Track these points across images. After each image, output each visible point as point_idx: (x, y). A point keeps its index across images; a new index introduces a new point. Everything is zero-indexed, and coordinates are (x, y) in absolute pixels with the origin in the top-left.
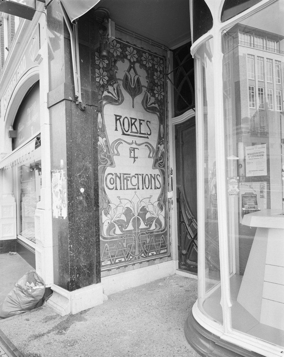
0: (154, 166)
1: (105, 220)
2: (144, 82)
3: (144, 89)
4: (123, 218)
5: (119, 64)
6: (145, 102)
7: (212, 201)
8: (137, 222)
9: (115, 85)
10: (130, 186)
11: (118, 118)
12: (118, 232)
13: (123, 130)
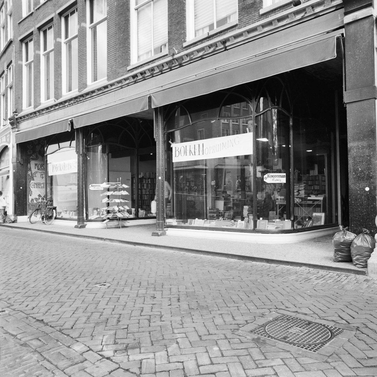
1: (30, 198)
4: (38, 197)
5: (37, 147)
9: (35, 154)
10: (40, 187)
11: (36, 165)
12: (35, 202)
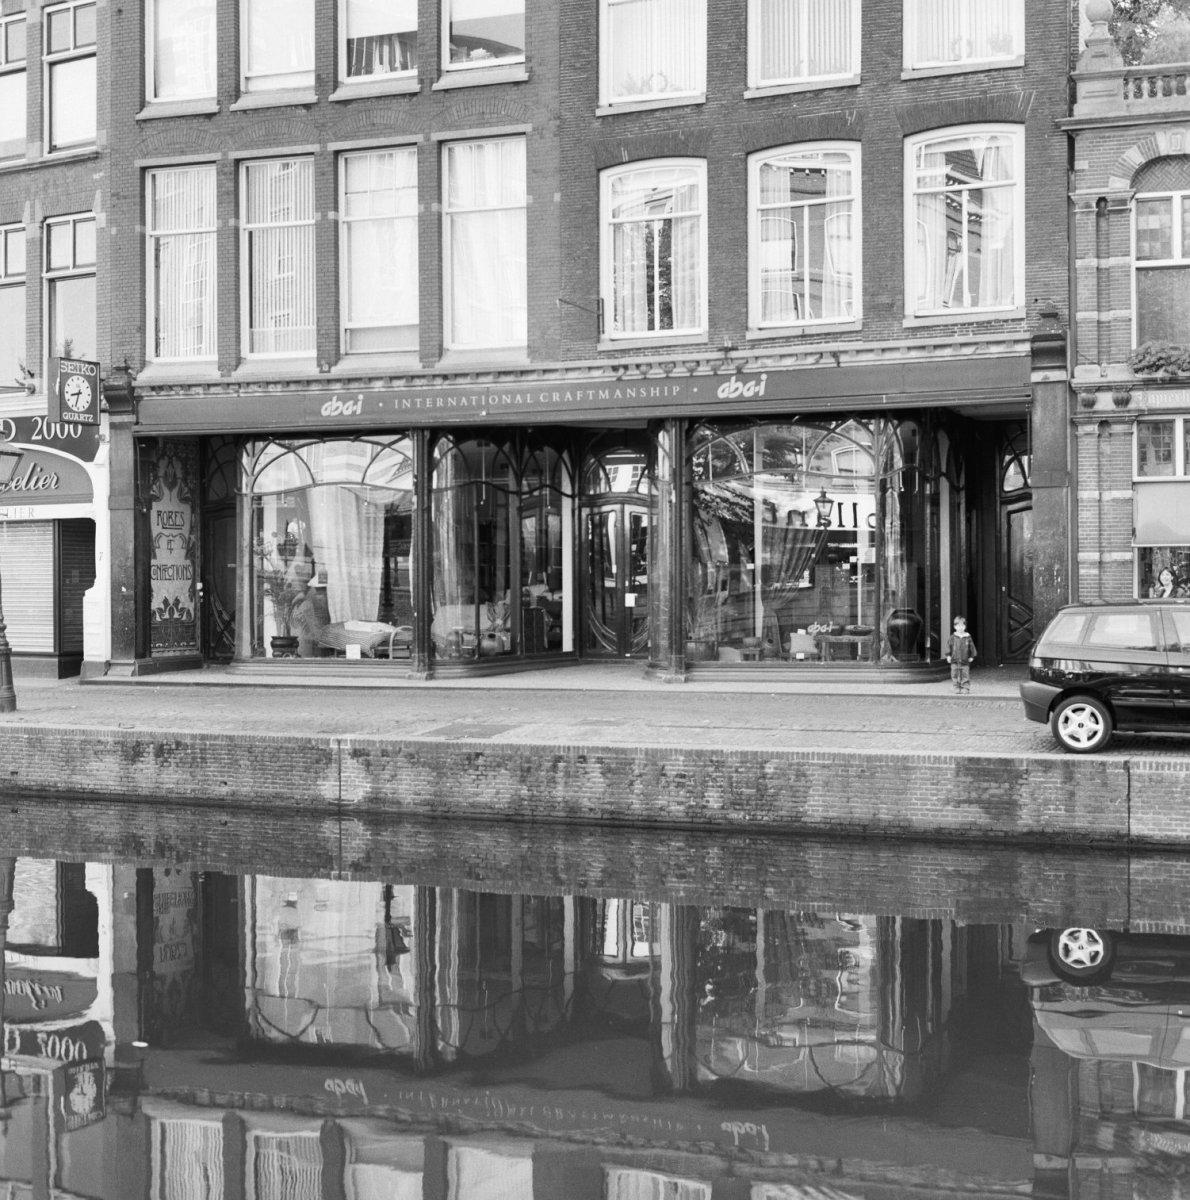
0: (186, 557)
2: (179, 474)
3: (179, 481)
4: (162, 606)
6: (180, 491)
7: (289, 725)
8: (171, 612)
13: (163, 523)
